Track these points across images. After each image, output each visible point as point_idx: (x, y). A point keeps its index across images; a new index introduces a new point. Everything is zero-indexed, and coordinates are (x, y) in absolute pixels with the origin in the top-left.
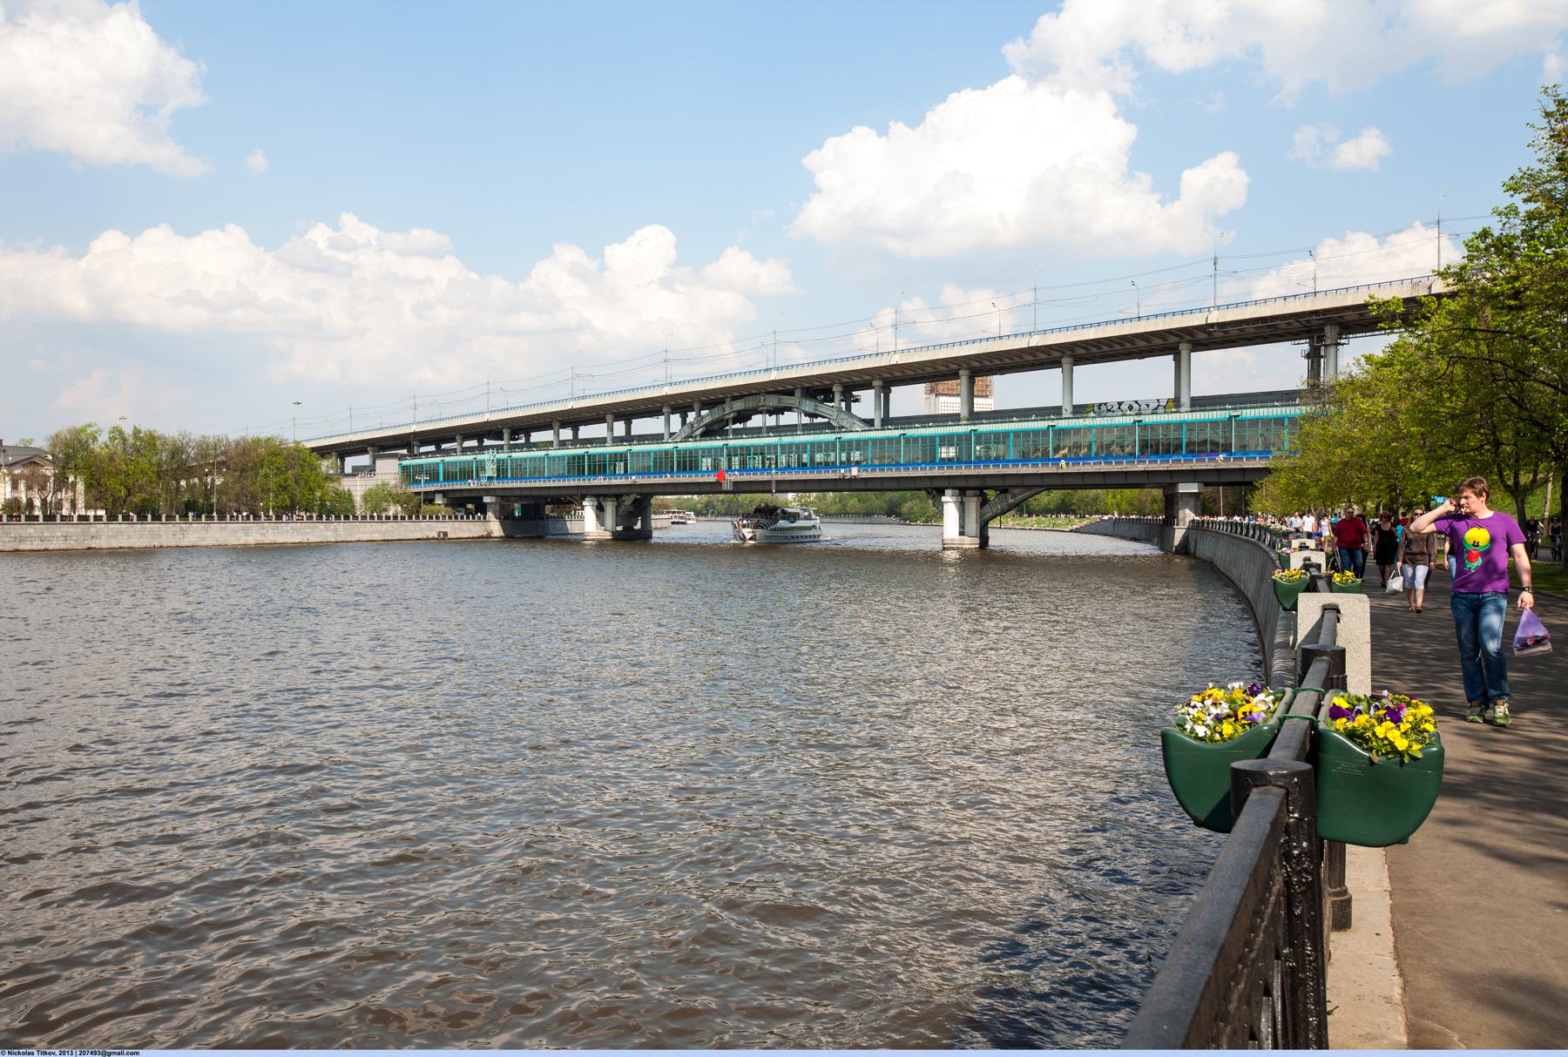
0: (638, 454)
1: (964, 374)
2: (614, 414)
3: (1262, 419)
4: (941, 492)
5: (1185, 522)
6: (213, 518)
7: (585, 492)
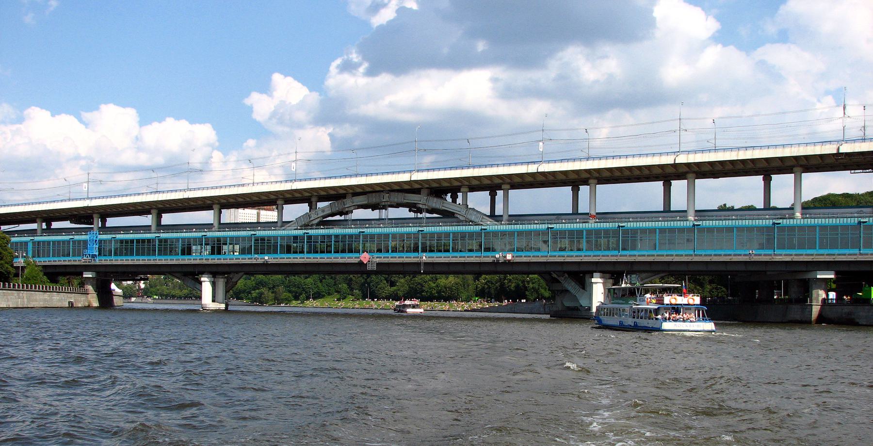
1: (154, 212)
2: (596, 178)
3: (797, 226)
5: (817, 300)
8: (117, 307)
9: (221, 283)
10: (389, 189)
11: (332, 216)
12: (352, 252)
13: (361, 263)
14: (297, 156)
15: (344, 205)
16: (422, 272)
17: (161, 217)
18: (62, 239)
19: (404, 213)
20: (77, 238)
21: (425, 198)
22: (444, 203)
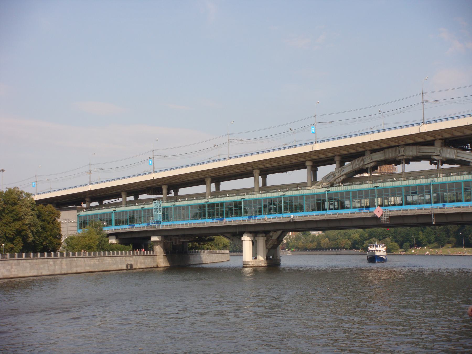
0: (179, 207)
4: (241, 234)
6: (14, 257)
7: (242, 230)
8: (192, 266)
9: (261, 241)
10: (403, 143)
11: (360, 174)
12: (120, 224)
13: (375, 218)
14: (154, 153)
15: (364, 162)
16: (434, 223)
17: (267, 177)
18: (125, 209)
19: (425, 165)
20: (147, 207)
21: (439, 149)
22: (458, 153)
